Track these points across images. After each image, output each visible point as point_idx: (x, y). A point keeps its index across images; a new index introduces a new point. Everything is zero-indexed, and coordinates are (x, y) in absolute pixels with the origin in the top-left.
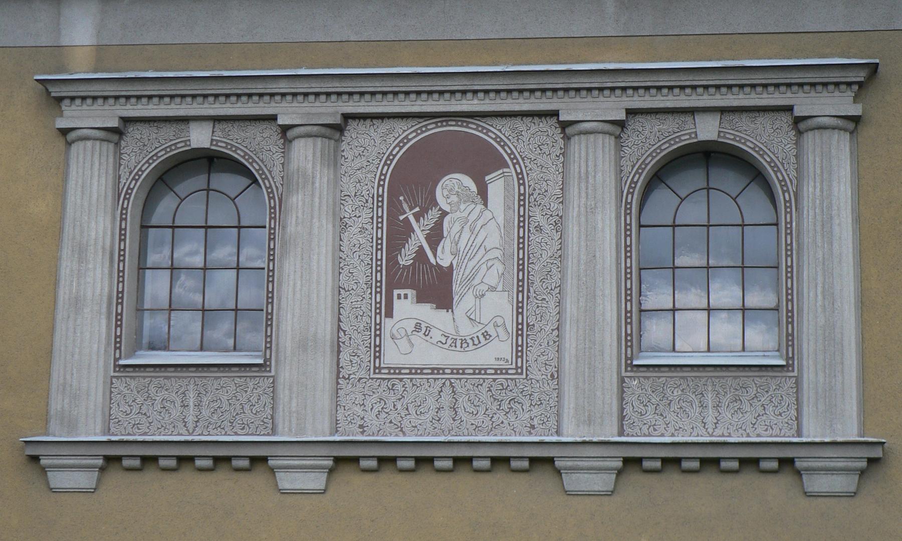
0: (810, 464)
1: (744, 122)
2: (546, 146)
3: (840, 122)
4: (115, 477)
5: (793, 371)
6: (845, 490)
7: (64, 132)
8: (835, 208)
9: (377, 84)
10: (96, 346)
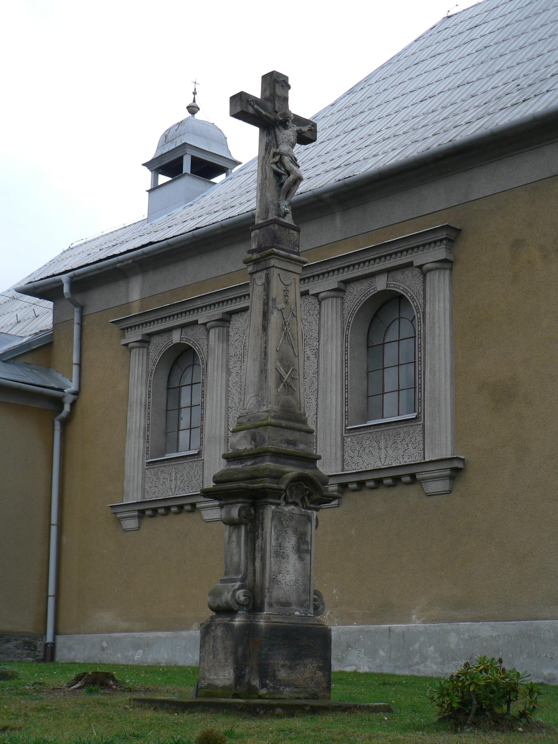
0: (422, 476)
1: (399, 276)
2: (311, 311)
3: (438, 265)
4: (147, 522)
5: (421, 420)
6: (444, 490)
7: (126, 345)
8: (437, 317)
9: (235, 293)
10: (137, 454)
